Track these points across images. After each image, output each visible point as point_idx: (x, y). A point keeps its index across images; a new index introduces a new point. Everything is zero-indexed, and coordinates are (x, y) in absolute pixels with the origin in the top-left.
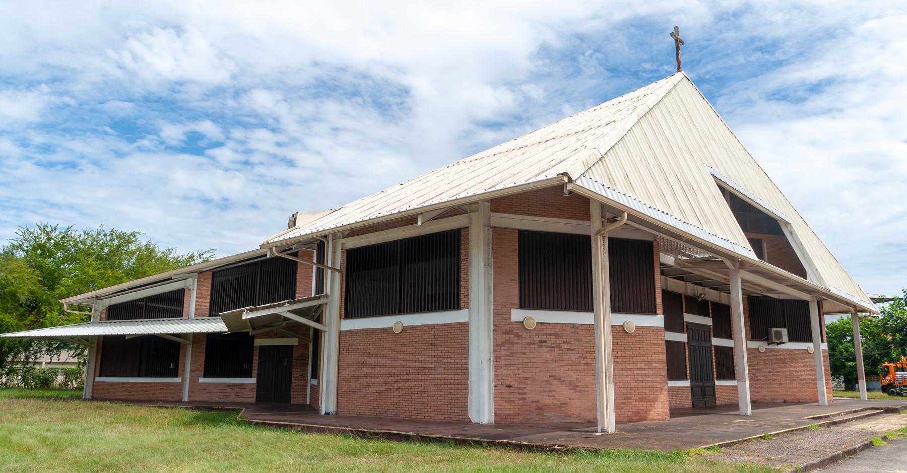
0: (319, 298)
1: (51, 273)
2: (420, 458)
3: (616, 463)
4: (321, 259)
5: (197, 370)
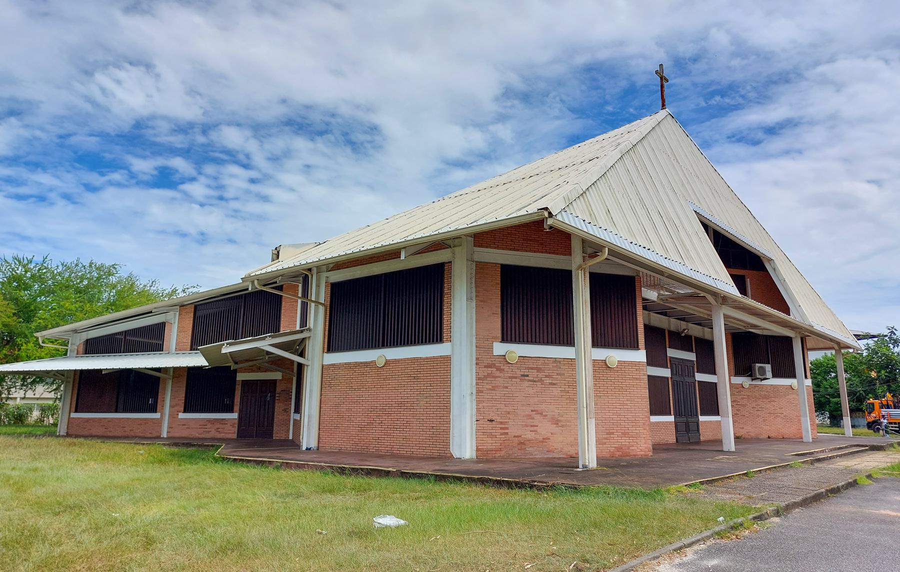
0: (302, 332)
1: (27, 306)
2: (398, 495)
3: (595, 501)
4: (305, 293)
5: (177, 405)
